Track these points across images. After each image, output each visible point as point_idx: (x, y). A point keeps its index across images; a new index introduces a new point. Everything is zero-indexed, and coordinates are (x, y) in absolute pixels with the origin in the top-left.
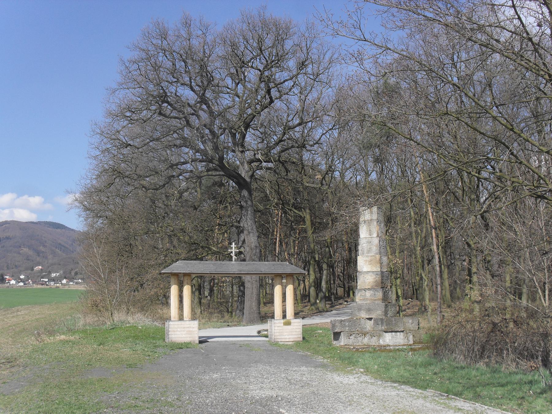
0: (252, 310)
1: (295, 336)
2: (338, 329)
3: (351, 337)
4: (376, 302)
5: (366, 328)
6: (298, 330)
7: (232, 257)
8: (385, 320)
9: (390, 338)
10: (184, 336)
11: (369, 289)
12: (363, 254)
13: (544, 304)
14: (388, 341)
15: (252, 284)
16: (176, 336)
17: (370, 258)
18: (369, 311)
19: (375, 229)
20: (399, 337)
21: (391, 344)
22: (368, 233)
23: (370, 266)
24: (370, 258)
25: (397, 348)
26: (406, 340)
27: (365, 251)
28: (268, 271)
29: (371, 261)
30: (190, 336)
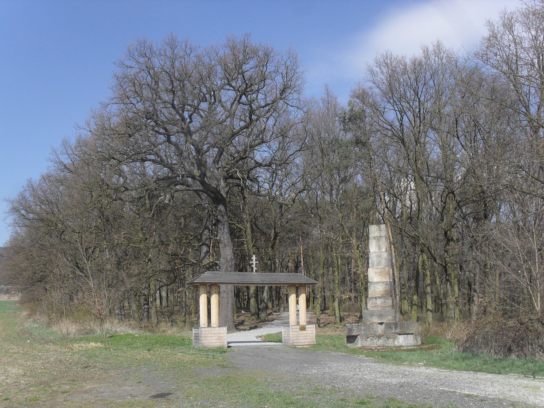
0: (228, 319)
1: (310, 340)
4: (387, 309)
7: (252, 268)
8: (399, 324)
9: (403, 340)
10: (214, 341)
12: (373, 266)
13: (537, 309)
14: (401, 342)
15: (228, 293)
16: (207, 341)
17: (380, 270)
19: (384, 245)
21: (403, 345)
22: (377, 248)
24: (380, 270)
25: (410, 348)
26: (415, 342)
27: (375, 264)
28: (285, 282)
29: (381, 272)
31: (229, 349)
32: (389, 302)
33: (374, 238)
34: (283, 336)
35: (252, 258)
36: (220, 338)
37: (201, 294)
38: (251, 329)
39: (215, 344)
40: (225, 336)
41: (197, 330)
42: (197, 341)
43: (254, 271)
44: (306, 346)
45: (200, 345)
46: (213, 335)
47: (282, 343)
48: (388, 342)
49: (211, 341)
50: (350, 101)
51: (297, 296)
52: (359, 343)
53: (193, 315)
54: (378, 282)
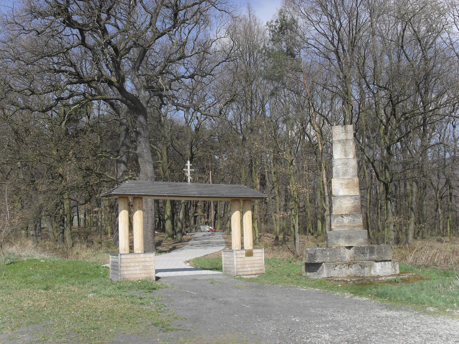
0: (147, 240)
1: (258, 269)
2: (320, 259)
3: (336, 268)
4: (356, 229)
5: (345, 258)
6: (260, 262)
7: (186, 177)
8: (376, 248)
9: (380, 268)
10: (138, 272)
11: (346, 215)
12: (338, 176)
14: (378, 271)
15: (148, 213)
16: (129, 272)
18: (349, 238)
20: (387, 266)
21: (381, 275)
22: (343, 153)
23: (347, 190)
24: (347, 181)
26: (394, 270)
27: (341, 173)
28: (229, 195)
29: (348, 184)
30: (145, 272)
31: (158, 283)
32: (360, 221)
33: (339, 141)
34: (223, 263)
35: (186, 165)
36: (145, 268)
37: (121, 210)
38: (170, 250)
39: (139, 276)
40: (152, 265)
41: (115, 257)
42: (115, 272)
43: (189, 181)
44: (253, 276)
45: (120, 278)
46: (137, 264)
47: (222, 271)
48: (362, 271)
49: (134, 272)
50: (281, 10)
51: (242, 214)
52: (324, 273)
53: (109, 235)
54: (345, 196)
